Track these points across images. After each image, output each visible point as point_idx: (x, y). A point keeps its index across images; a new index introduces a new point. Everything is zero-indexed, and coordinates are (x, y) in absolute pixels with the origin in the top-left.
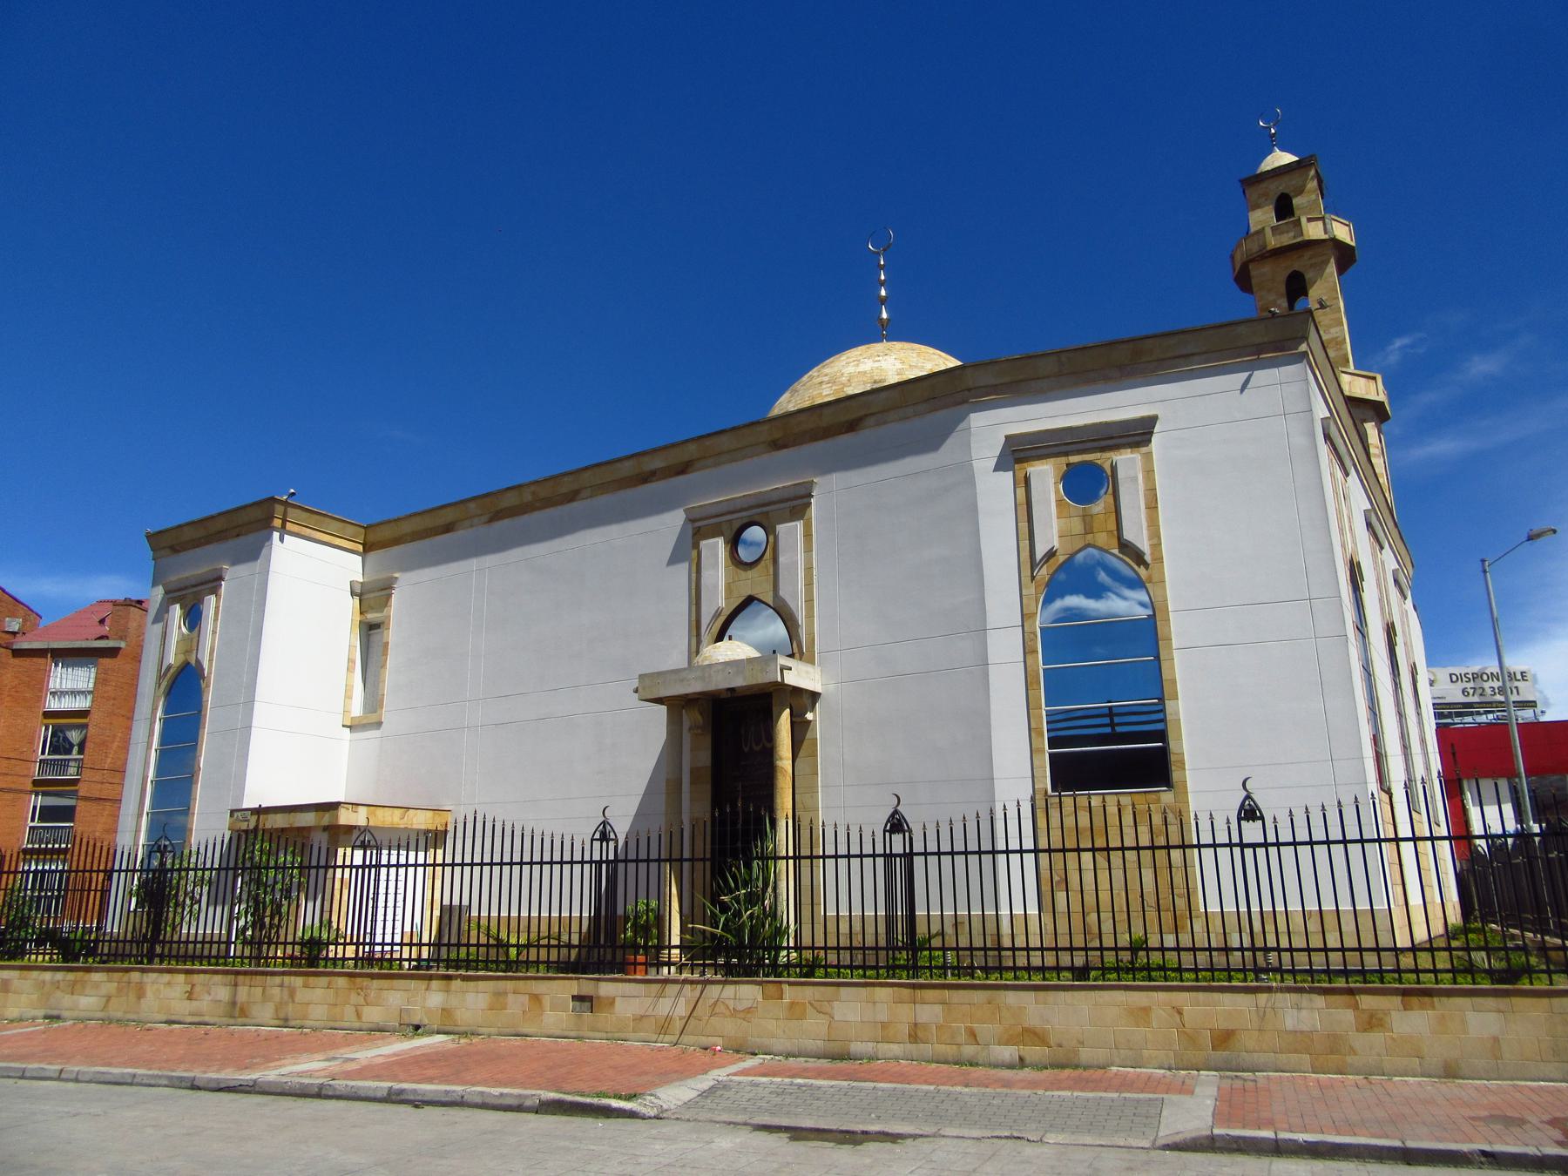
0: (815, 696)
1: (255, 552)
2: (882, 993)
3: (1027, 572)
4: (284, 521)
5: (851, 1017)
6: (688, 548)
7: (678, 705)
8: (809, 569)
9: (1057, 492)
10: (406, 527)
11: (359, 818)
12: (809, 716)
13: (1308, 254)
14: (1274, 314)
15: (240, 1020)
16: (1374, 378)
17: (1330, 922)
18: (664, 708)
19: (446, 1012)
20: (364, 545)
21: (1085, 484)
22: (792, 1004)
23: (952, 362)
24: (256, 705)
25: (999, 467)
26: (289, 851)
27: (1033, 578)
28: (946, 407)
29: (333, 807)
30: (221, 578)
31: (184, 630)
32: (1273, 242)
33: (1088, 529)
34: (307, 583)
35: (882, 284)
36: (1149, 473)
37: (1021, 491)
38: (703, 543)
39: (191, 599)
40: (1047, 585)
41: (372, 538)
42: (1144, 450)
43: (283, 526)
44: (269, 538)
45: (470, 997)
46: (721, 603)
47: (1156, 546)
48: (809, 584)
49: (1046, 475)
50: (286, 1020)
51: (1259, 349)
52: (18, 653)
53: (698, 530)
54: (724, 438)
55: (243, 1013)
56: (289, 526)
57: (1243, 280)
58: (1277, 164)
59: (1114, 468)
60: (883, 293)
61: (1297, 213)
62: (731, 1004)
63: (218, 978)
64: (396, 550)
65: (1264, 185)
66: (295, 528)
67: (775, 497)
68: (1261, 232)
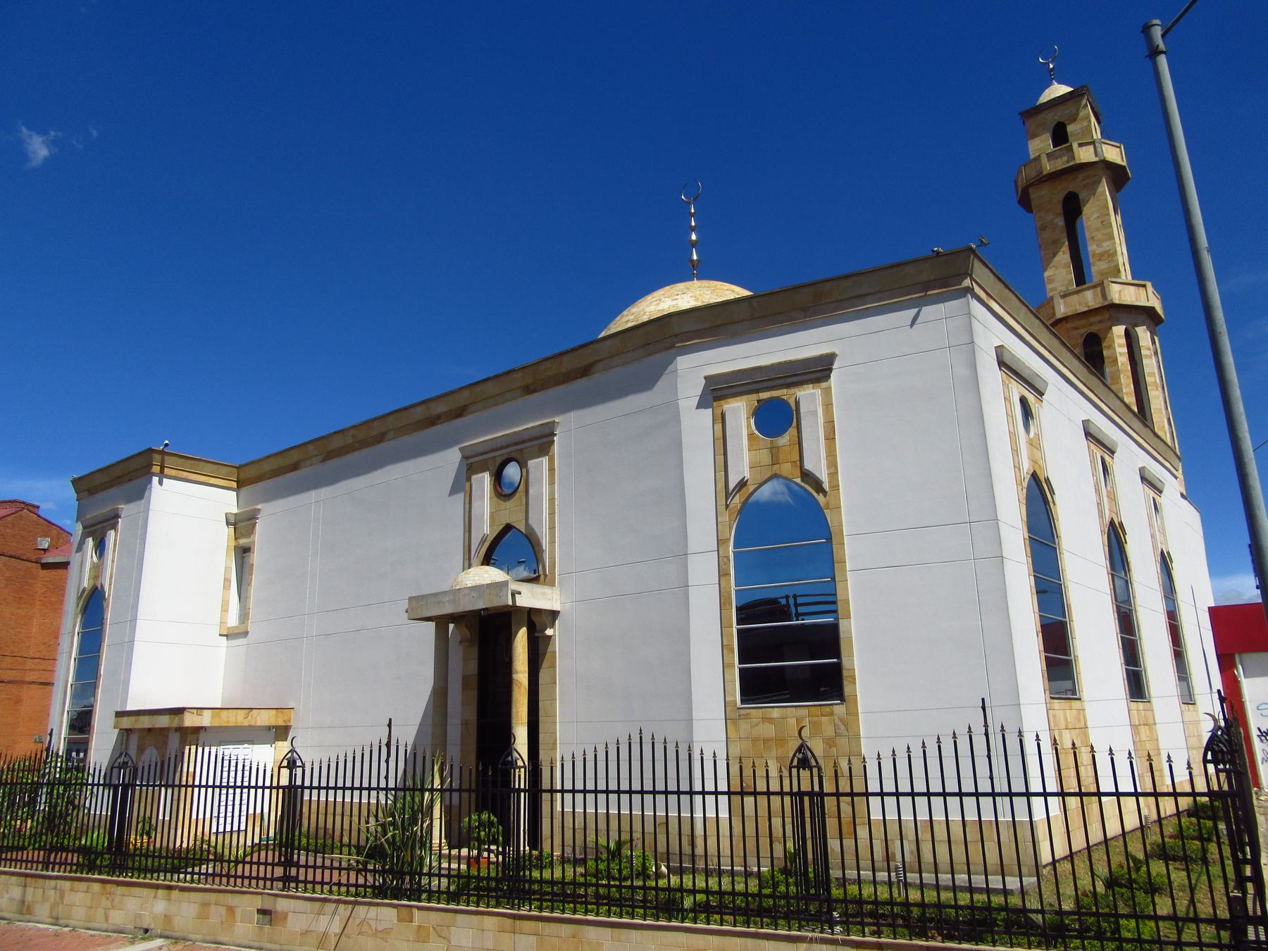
0: (554, 614)
1: (140, 493)
2: (489, 922)
3: (722, 501)
4: (162, 468)
5: (464, 943)
6: (461, 485)
7: (441, 622)
8: (552, 500)
9: (749, 426)
10: (267, 467)
11: (206, 720)
12: (549, 632)
13: (1081, 176)
14: (938, 253)
15: (27, 917)
16: (1144, 286)
17: (990, 834)
18: (432, 625)
19: (168, 918)
20: (238, 482)
21: (776, 419)
22: (419, 927)
23: (746, 293)
24: (138, 622)
25: (702, 404)
26: (161, 743)
27: (727, 506)
28: (660, 351)
29: (179, 711)
30: (118, 516)
31: (95, 559)
32: (1048, 167)
33: (775, 461)
34: (185, 520)
35: (693, 229)
36: (828, 406)
37: (719, 426)
38: (474, 477)
39: (98, 530)
40: (740, 512)
41: (242, 476)
42: (824, 385)
43: (162, 471)
44: (150, 482)
45: (184, 905)
46: (487, 530)
47: (833, 475)
48: (552, 513)
49: (739, 411)
50: (57, 919)
51: (927, 286)
52: (46, 566)
53: (471, 465)
54: (490, 384)
55: (29, 912)
56: (167, 471)
57: (1025, 201)
58: (1053, 96)
59: (797, 403)
60: (694, 237)
61: (1071, 139)
62: (373, 924)
63: (14, 879)
64: (260, 485)
65: (1042, 115)
66: (173, 473)
67: (526, 436)
68: (1038, 158)
